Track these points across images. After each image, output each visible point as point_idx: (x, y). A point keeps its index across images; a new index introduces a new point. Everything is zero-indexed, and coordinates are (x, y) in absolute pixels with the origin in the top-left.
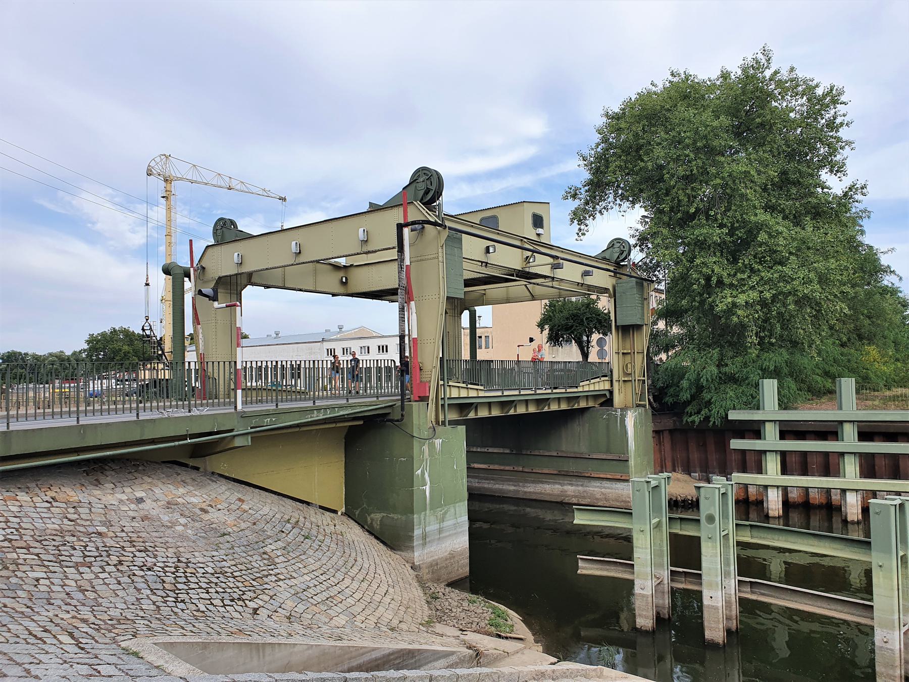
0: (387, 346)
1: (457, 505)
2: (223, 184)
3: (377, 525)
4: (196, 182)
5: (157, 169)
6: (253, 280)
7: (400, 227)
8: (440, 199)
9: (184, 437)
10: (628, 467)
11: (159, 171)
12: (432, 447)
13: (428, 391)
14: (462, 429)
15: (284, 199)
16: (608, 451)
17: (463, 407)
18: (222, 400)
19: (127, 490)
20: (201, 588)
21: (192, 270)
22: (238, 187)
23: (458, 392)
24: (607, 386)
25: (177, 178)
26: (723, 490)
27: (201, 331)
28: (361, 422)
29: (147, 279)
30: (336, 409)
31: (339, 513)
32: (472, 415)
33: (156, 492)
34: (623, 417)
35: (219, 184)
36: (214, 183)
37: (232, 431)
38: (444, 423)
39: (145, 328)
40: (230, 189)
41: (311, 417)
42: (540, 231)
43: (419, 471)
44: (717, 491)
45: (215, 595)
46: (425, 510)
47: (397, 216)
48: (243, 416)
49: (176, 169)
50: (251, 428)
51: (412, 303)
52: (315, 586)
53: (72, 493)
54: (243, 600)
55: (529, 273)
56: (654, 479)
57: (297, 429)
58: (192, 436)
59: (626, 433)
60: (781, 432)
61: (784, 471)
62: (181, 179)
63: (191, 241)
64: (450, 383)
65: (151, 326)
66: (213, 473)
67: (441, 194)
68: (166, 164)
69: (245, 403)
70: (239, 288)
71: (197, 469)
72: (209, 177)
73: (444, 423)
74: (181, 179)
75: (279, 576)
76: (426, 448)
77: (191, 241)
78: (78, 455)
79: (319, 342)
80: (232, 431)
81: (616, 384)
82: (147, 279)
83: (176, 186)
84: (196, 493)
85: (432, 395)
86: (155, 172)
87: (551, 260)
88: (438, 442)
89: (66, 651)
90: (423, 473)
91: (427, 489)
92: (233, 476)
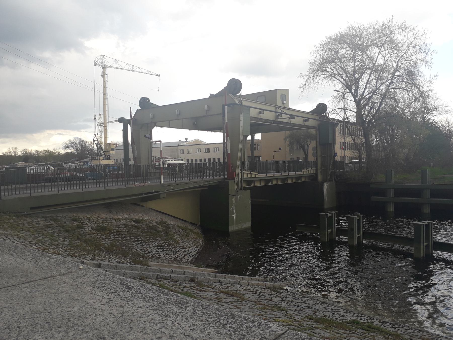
0: (209, 149)
2: (130, 69)
4: (117, 68)
5: (99, 62)
6: (156, 125)
7: (224, 106)
8: (240, 92)
9: (142, 194)
11: (100, 63)
13: (235, 176)
14: (249, 192)
15: (159, 76)
17: (249, 182)
18: (145, 178)
19: (121, 214)
20: (155, 250)
21: (131, 120)
22: (137, 70)
23: (247, 175)
25: (108, 66)
26: (358, 218)
29: (95, 116)
30: (198, 183)
31: (198, 225)
32: (252, 185)
33: (132, 215)
35: (128, 69)
36: (126, 68)
37: (159, 192)
38: (241, 189)
39: (95, 140)
40: (133, 71)
41: (188, 186)
43: (232, 208)
44: (355, 218)
45: (161, 253)
46: (234, 225)
48: (163, 185)
49: (108, 62)
50: (167, 190)
52: (194, 251)
53: (103, 215)
54: (171, 255)
55: (279, 122)
56: (330, 213)
58: (145, 194)
62: (110, 67)
64: (244, 172)
65: (97, 139)
66: (149, 208)
67: (241, 90)
68: (102, 59)
69: (164, 181)
71: (143, 206)
72: (123, 65)
73: (241, 189)
74: (110, 67)
75: (181, 247)
76: (234, 199)
78: (104, 201)
80: (159, 192)
82: (95, 116)
83: (108, 70)
84: (146, 216)
85: (236, 177)
86: (98, 64)
87: (288, 116)
88: (239, 197)
91: (235, 216)
92: (157, 210)
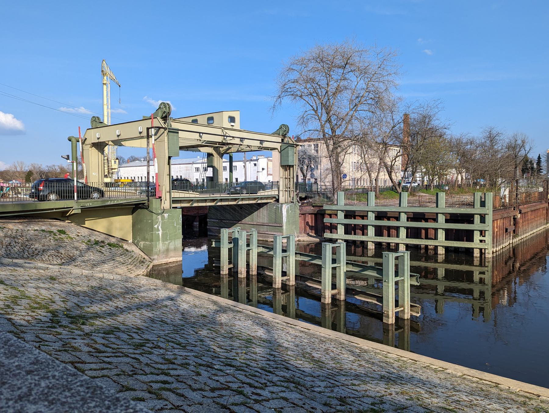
1: (176, 240)
3: (142, 246)
9: (53, 209)
10: (282, 229)
12: (163, 218)
16: (275, 223)
24: (277, 193)
27: (85, 166)
28: (134, 206)
34: (281, 207)
42: (233, 124)
46: (159, 241)
47: (148, 124)
51: (156, 159)
57: (103, 208)
58: (56, 209)
59: (282, 214)
60: (345, 215)
61: (447, 239)
63: (79, 127)
70: (102, 147)
77: (79, 127)
79: (191, 164)
80: (72, 207)
81: (281, 193)
89: (296, 405)
90: (158, 227)
